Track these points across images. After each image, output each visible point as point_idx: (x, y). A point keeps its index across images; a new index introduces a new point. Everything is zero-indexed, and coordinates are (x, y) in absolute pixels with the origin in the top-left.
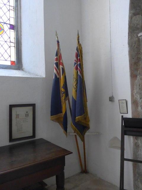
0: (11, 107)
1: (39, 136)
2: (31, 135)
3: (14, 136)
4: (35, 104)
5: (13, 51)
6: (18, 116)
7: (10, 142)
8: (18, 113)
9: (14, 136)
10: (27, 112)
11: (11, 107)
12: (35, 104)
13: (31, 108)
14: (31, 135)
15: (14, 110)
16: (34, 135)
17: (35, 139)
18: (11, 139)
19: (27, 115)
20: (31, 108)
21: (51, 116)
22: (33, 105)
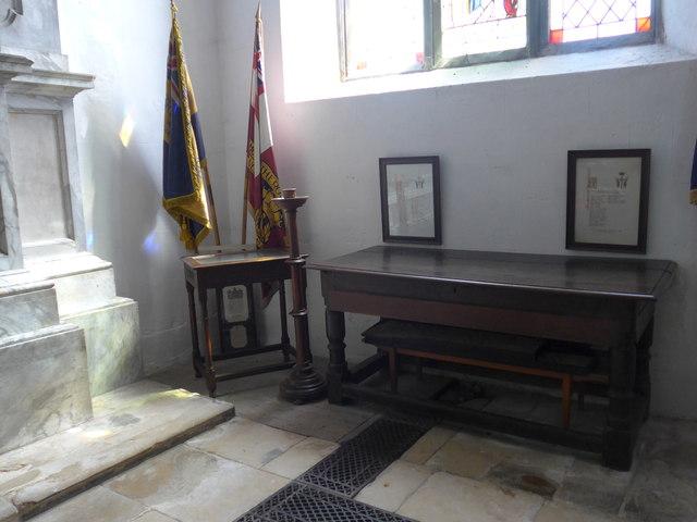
0: (574, 157)
1: (652, 254)
2: (633, 241)
3: (581, 236)
4: (380, 159)
5: (588, 33)
6: (592, 182)
7: (567, 247)
8: (593, 175)
9: (581, 236)
10: (622, 174)
11: (574, 157)
12: (380, 159)
13: (637, 161)
14: (633, 241)
15: (583, 166)
16: (642, 245)
17: (438, 247)
18: (571, 242)
19: (622, 182)
20: (637, 161)
21: (692, 188)
22: (644, 155)
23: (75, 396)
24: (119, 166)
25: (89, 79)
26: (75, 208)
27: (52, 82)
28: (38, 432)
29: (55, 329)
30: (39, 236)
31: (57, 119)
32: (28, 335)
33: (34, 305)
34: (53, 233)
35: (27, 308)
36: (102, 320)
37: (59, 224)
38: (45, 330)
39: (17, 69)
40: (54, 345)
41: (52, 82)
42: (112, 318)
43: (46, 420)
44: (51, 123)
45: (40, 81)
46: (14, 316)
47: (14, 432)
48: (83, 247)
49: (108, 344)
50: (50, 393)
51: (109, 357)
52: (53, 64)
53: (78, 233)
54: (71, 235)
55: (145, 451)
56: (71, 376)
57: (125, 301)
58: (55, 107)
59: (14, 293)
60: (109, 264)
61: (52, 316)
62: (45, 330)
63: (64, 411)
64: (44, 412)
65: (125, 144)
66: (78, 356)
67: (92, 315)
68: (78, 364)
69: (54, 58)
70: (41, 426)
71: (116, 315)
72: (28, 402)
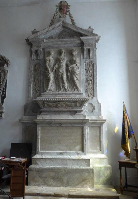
21: (122, 144)
23: (90, 182)
24: (112, 136)
25: (105, 120)
26: (102, 145)
27: (98, 121)
28: (83, 186)
29: (89, 168)
30: (94, 150)
31: (100, 128)
32: (83, 167)
33: (86, 162)
34: (97, 149)
35: (84, 162)
36: (103, 169)
37: (99, 148)
38: (87, 167)
39: (87, 121)
40: (87, 170)
41: (98, 121)
42: (105, 169)
43: (84, 184)
44: (99, 128)
45: (96, 122)
46: (82, 163)
47: (78, 184)
48: (103, 153)
49: (104, 174)
50: (85, 180)
51: (103, 177)
52: (99, 118)
53: (102, 150)
54: (101, 150)
55: (94, 196)
56: (90, 177)
57: (109, 166)
58: (99, 126)
59: (83, 159)
60: (107, 157)
61: (89, 165)
62: (87, 167)
63: (88, 184)
64: (84, 183)
65: (116, 132)
66: (92, 174)
67: (101, 167)
68: (92, 175)
69: (100, 117)
70: (83, 185)
71: (106, 168)
72: (81, 180)
